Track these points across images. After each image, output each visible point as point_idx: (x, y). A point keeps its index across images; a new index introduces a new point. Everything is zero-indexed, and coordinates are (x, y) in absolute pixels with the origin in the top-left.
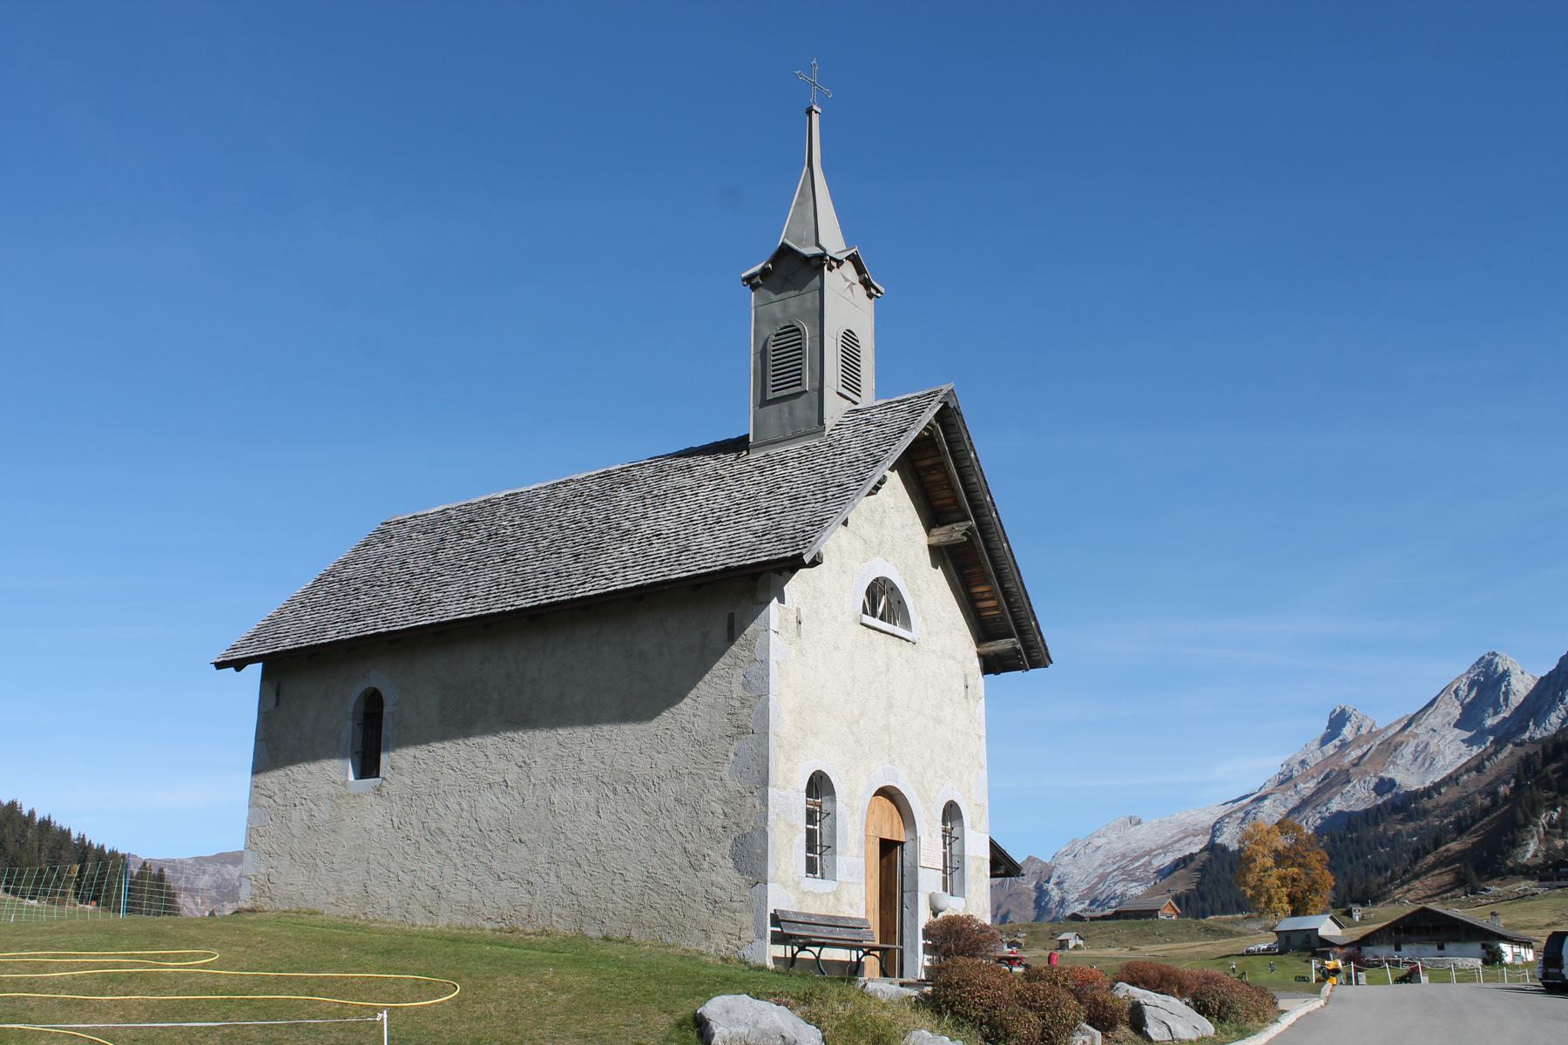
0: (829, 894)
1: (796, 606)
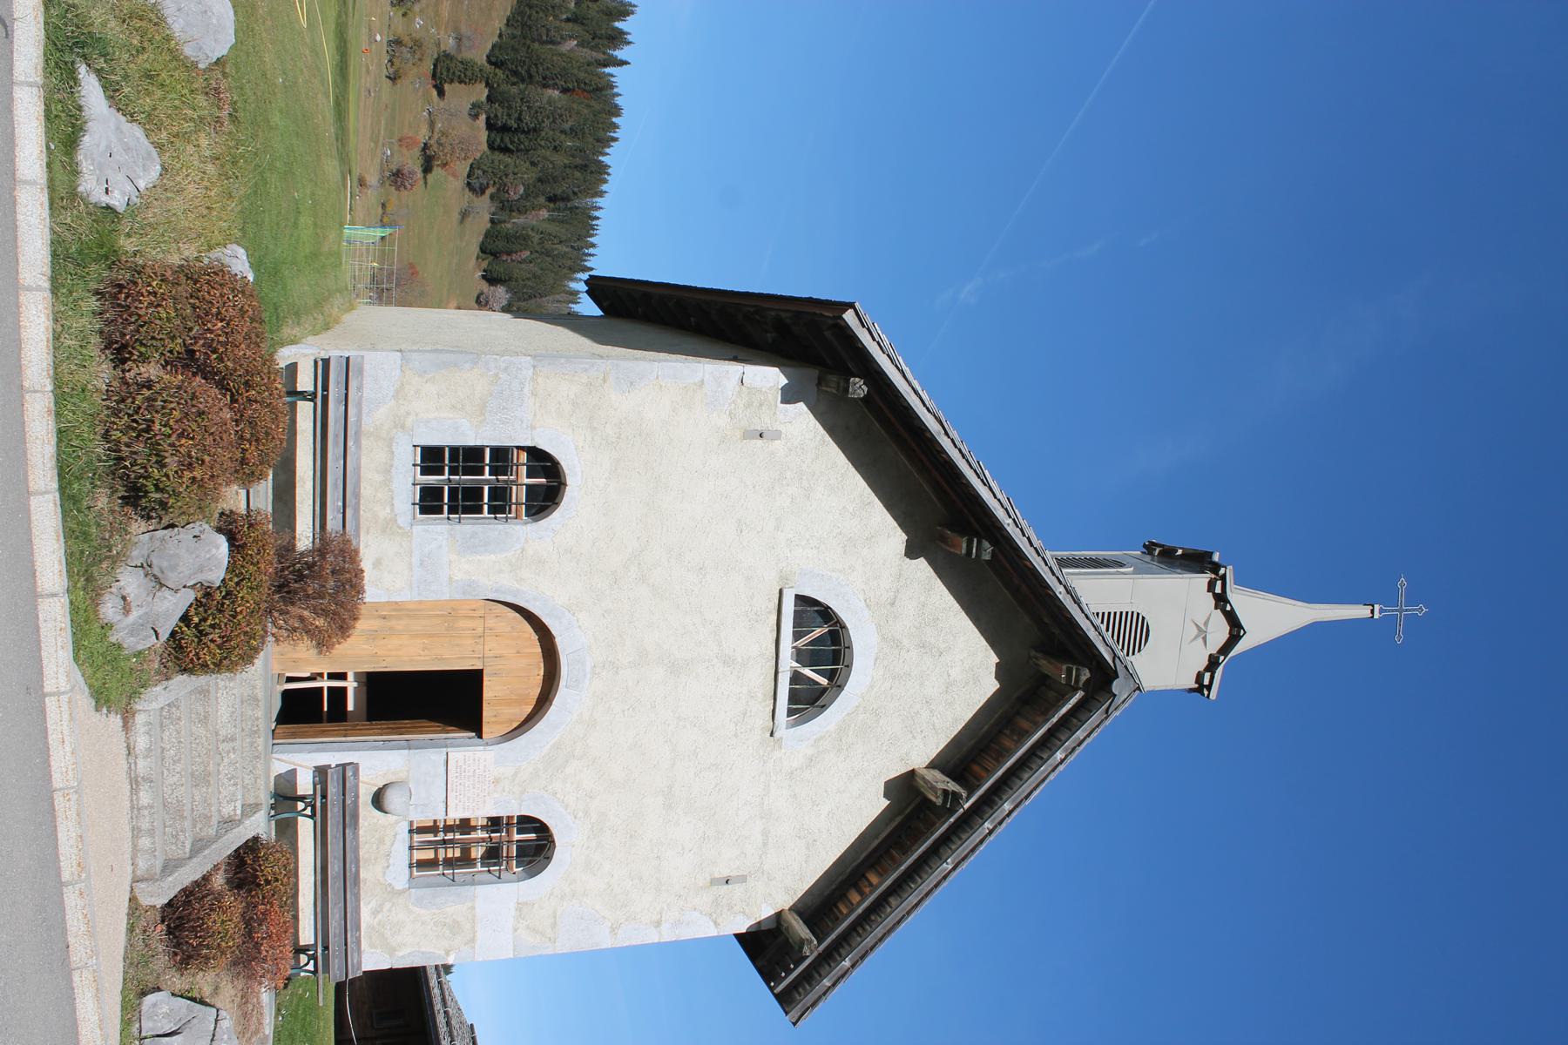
0: (392, 510)
1: (782, 428)
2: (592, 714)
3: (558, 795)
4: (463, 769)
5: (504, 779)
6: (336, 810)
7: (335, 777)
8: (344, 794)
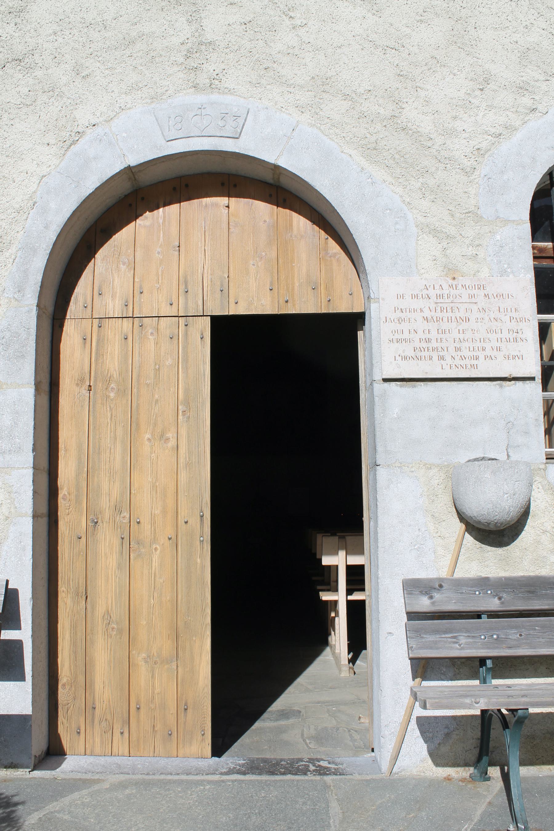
2: (302, 87)
3: (484, 145)
4: (424, 345)
5: (446, 256)
6: (513, 635)
7: (430, 638)
8: (478, 615)
